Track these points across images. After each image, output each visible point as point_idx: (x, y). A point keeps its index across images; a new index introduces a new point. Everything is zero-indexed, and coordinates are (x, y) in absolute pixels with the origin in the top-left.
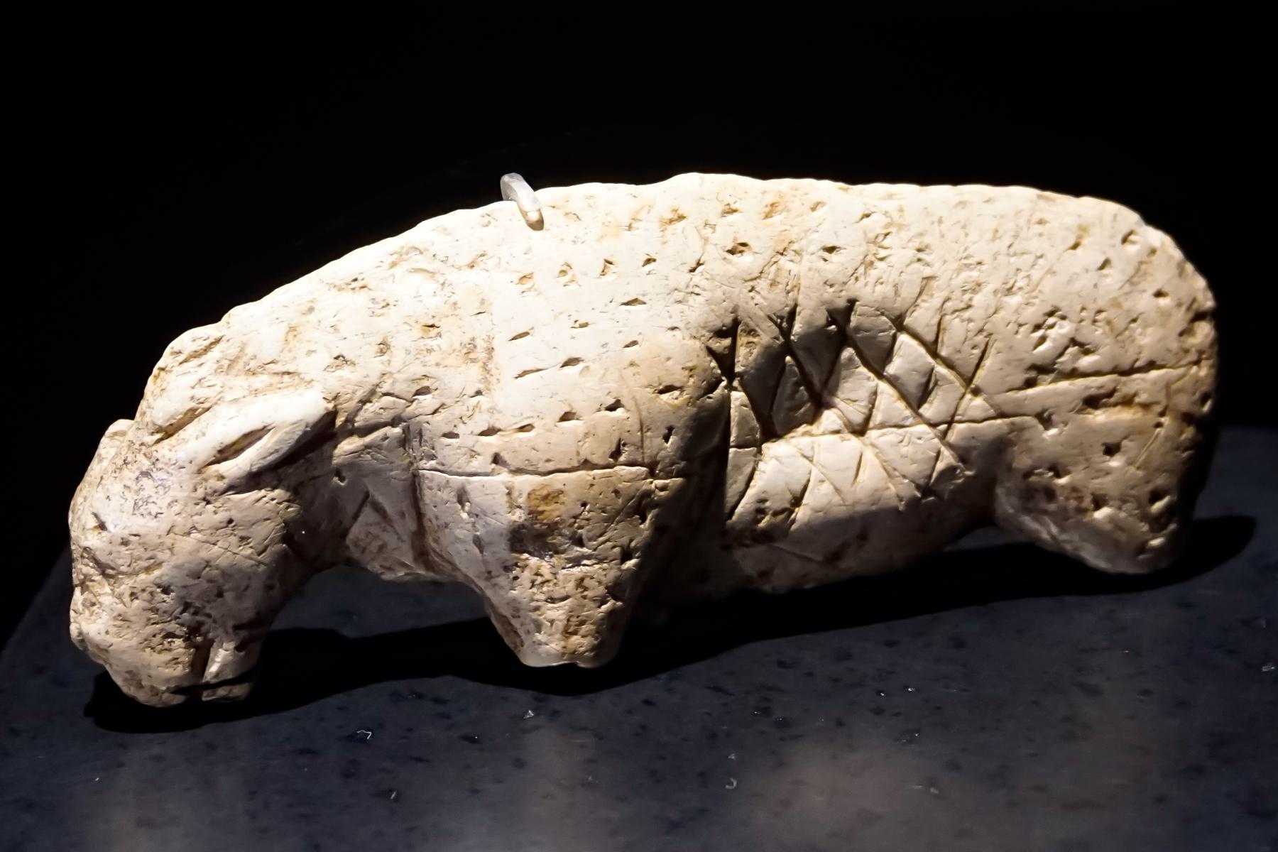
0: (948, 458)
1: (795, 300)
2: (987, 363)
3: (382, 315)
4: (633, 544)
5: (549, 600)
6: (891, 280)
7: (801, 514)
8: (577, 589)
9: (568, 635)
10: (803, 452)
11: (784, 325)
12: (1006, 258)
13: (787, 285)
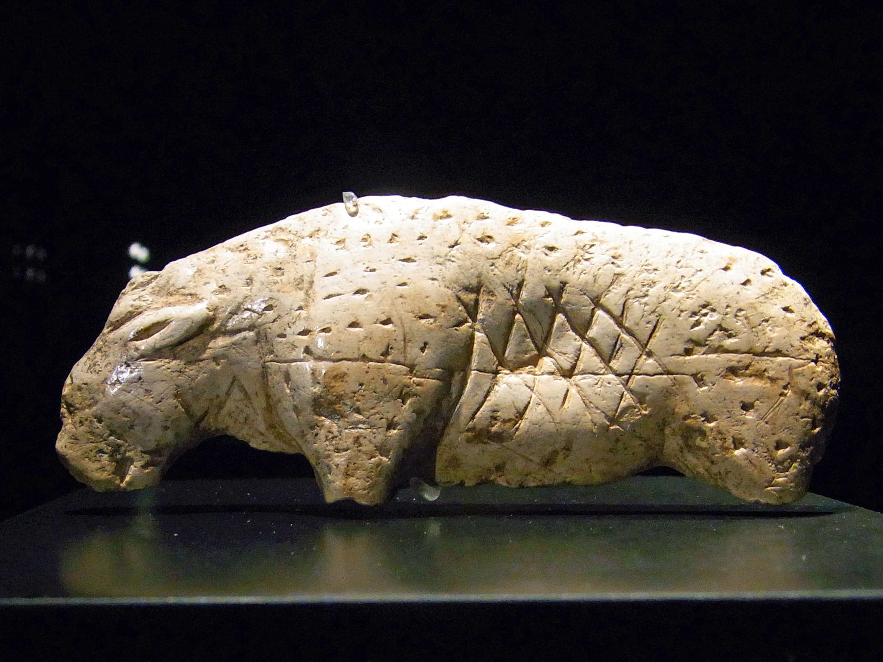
0: (628, 399)
1: (523, 276)
2: (657, 334)
3: (253, 263)
4: (396, 419)
5: (336, 450)
6: (592, 272)
7: (523, 424)
8: (354, 445)
9: (347, 476)
10: (526, 383)
11: (514, 292)
12: (675, 268)
13: (518, 266)
